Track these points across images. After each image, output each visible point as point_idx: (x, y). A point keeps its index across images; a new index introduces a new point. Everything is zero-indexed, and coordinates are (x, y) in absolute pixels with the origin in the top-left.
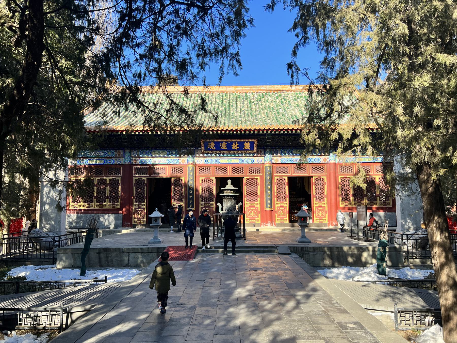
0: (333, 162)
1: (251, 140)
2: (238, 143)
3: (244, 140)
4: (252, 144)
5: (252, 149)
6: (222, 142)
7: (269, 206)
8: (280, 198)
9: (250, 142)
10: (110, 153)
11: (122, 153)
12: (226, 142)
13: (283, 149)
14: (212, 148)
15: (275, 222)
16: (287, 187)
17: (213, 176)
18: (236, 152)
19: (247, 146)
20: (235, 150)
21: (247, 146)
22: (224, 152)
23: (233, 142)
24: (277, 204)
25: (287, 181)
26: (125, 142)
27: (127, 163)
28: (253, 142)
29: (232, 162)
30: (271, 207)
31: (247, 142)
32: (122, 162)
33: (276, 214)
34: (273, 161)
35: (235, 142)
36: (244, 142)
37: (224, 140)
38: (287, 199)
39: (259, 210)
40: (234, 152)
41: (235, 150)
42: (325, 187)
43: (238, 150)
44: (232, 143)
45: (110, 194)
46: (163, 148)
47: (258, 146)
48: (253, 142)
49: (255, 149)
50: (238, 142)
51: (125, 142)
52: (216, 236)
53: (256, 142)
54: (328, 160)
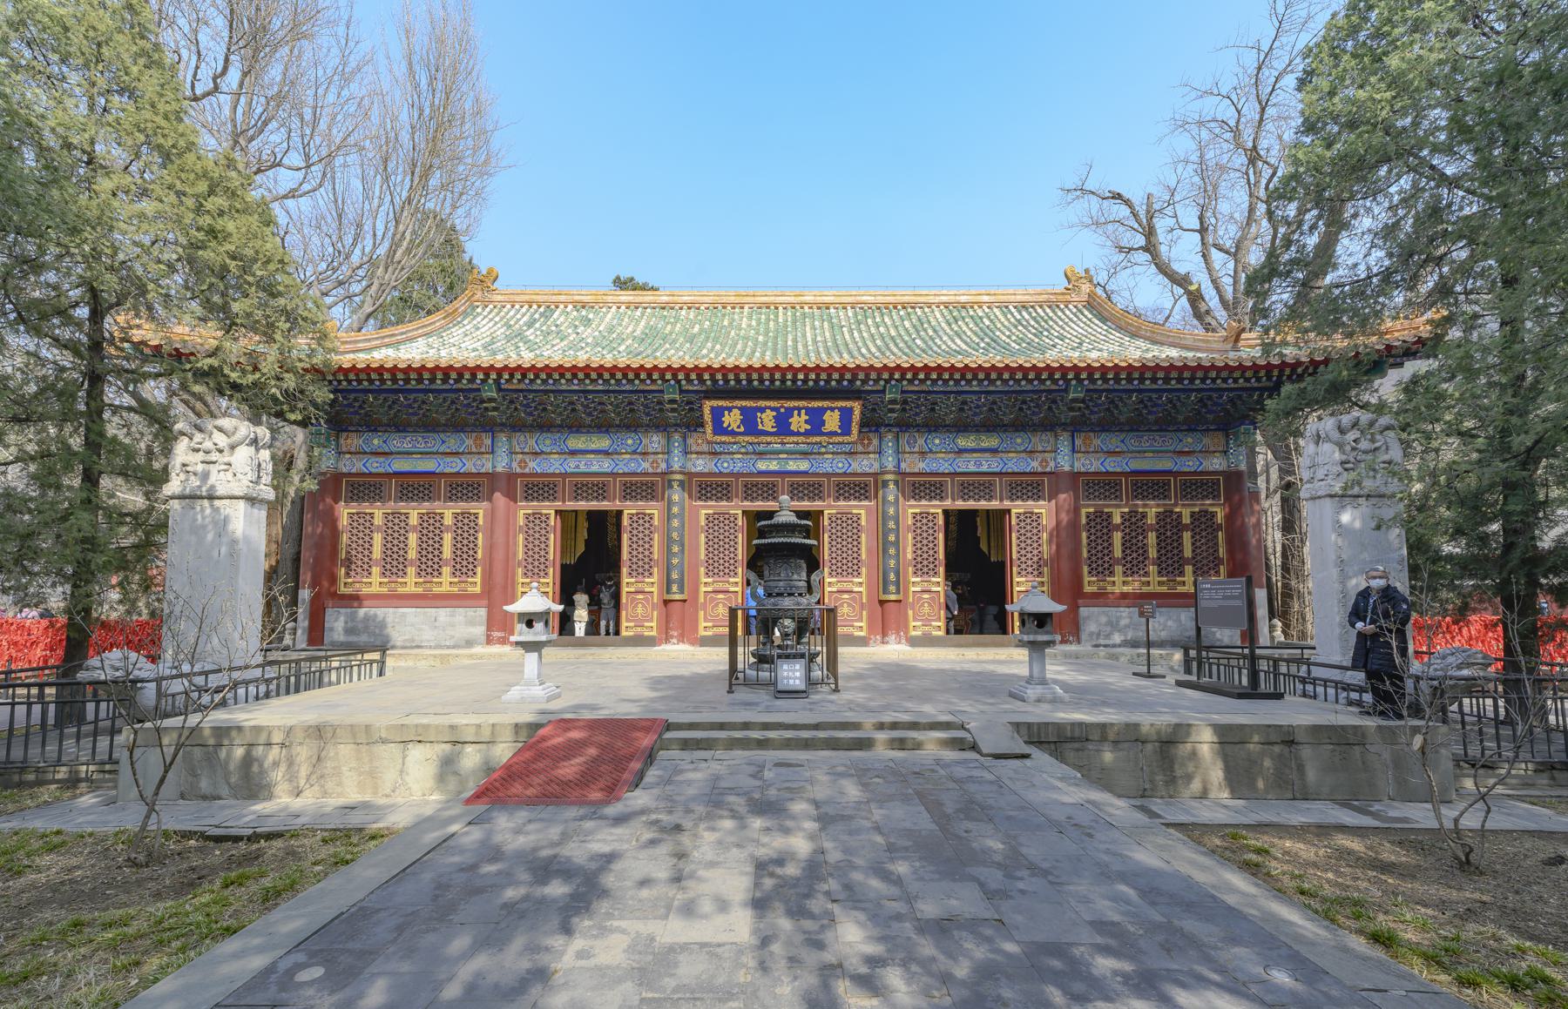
0: (1067, 468)
1: (744, 403)
2: (809, 411)
3: (825, 404)
4: (846, 415)
5: (845, 428)
6: (762, 410)
7: (892, 588)
8: (923, 568)
9: (840, 409)
10: (376, 442)
11: (875, 442)
12: (772, 409)
13: (930, 432)
14: (734, 426)
15: (906, 633)
16: (941, 536)
17: (737, 507)
18: (801, 439)
19: (832, 421)
20: (798, 434)
21: (832, 421)
22: (769, 439)
23: (795, 408)
24: (915, 583)
25: (941, 521)
26: (673, 410)
27: (499, 469)
28: (851, 409)
29: (419, 469)
30: (898, 592)
31: (832, 409)
32: (488, 468)
33: (910, 612)
34: (903, 465)
35: (799, 409)
36: (824, 410)
37: (768, 403)
38: (942, 570)
39: (702, 613)
40: (795, 439)
41: (798, 434)
42: (521, 556)
43: (807, 433)
44: (790, 412)
45: (1181, 537)
46: (569, 428)
47: (862, 425)
48: (851, 409)
49: (855, 430)
50: (807, 409)
51: (673, 410)
52: (741, 675)
53: (857, 407)
54: (1052, 464)
